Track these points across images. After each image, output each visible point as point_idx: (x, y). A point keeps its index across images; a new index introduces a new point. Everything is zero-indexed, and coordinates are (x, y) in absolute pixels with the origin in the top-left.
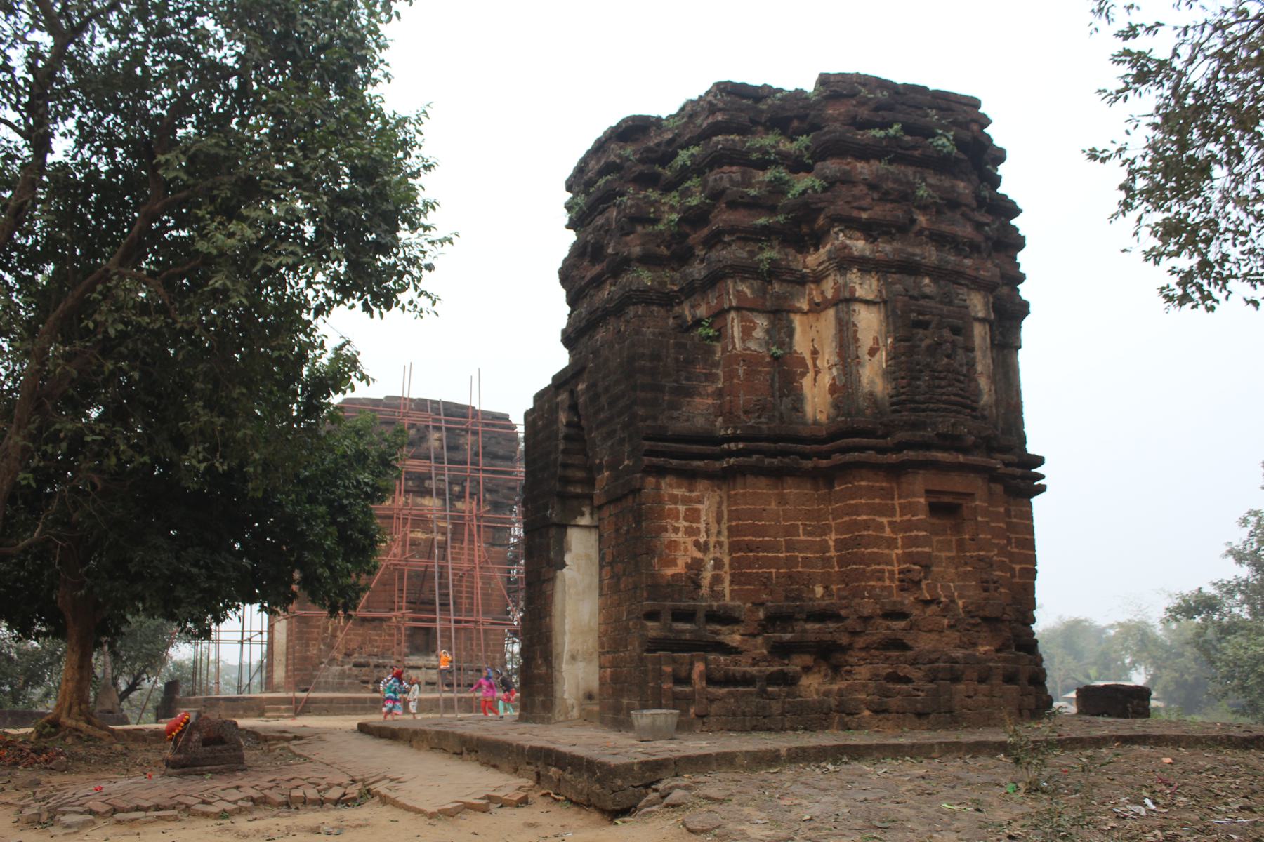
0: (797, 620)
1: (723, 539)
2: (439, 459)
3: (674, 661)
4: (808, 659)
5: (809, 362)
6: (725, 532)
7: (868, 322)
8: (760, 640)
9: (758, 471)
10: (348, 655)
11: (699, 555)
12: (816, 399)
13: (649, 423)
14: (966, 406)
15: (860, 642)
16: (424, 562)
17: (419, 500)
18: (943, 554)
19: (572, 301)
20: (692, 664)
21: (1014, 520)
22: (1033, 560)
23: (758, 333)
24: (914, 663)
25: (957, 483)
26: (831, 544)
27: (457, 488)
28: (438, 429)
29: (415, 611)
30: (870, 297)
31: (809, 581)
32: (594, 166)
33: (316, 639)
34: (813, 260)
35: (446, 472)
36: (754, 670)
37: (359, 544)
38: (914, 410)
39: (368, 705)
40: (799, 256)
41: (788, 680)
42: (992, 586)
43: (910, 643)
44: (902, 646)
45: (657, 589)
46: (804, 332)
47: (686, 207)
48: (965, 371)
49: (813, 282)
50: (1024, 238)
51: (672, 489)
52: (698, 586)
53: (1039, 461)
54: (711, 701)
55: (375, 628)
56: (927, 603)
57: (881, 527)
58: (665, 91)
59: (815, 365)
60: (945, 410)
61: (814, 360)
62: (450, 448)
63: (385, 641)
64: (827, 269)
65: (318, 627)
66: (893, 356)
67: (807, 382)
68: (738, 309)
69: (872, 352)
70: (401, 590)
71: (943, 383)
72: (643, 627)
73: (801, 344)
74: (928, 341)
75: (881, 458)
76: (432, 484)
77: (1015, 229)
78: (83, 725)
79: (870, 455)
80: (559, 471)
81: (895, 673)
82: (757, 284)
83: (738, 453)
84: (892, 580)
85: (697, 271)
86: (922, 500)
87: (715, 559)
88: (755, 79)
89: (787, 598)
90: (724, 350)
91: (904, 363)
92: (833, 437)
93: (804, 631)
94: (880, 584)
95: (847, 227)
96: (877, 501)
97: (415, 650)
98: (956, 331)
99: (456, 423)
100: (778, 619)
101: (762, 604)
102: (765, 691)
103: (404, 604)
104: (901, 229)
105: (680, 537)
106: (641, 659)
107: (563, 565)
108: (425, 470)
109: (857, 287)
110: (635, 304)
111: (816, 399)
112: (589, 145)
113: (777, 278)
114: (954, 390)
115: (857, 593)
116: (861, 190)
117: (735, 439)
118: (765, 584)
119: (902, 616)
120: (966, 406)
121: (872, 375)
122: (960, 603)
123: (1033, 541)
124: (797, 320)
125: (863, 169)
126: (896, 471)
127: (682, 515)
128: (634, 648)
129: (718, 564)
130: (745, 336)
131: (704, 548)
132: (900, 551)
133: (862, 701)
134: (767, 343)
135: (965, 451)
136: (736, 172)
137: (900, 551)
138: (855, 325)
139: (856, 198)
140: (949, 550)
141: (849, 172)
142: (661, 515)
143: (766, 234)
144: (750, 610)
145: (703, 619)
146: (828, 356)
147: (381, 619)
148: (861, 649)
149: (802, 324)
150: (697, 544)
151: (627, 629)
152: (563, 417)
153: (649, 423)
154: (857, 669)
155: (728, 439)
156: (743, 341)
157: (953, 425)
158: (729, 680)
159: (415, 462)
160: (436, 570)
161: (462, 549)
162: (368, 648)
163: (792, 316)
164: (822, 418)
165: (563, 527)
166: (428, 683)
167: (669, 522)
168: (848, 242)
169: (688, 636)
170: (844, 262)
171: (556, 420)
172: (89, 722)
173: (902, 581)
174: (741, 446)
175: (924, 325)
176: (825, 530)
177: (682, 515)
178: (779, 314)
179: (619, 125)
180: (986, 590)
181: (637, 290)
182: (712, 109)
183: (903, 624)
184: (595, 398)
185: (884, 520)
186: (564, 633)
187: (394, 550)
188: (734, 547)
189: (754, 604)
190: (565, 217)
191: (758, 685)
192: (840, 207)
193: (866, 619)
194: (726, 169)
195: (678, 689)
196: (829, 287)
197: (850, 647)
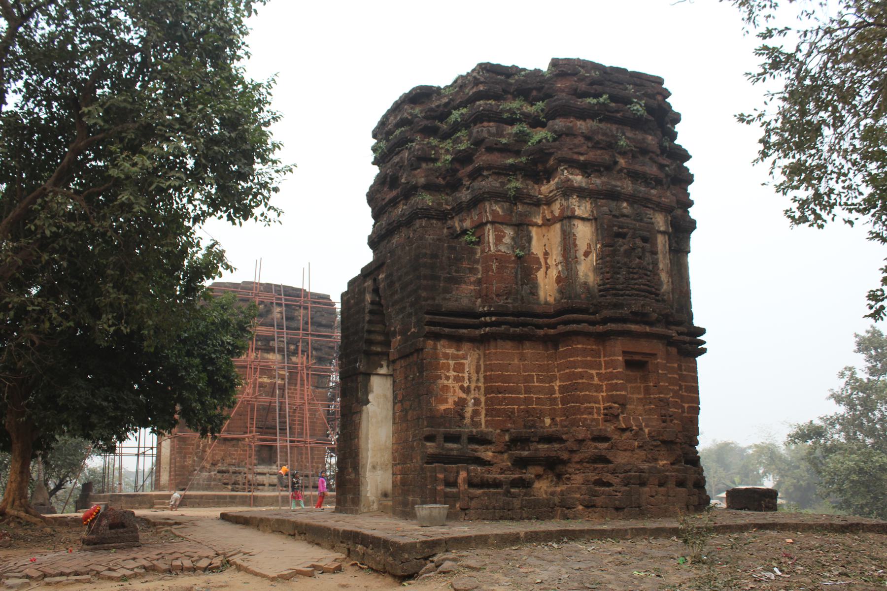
0: (532, 442)
2: (280, 326)
3: (445, 470)
4: (539, 470)
5: (542, 261)
6: (482, 380)
7: (584, 233)
8: (506, 456)
11: (464, 396)
12: (547, 286)
13: (429, 302)
14: (651, 293)
15: (576, 457)
16: (268, 399)
17: (266, 355)
19: (376, 216)
20: (458, 473)
23: (507, 240)
24: (614, 472)
25: (644, 346)
26: (557, 388)
27: (292, 347)
28: (280, 305)
30: (585, 215)
31: (541, 414)
32: (392, 120)
33: (191, 453)
34: (546, 189)
36: (502, 477)
39: (228, 500)
40: (536, 186)
41: (526, 484)
43: (611, 459)
44: (605, 460)
45: (434, 419)
46: (539, 240)
49: (545, 204)
51: (445, 349)
53: (702, 331)
54: (472, 499)
55: (233, 446)
56: (623, 430)
57: (591, 377)
59: (546, 263)
61: (546, 259)
65: (193, 445)
66: (600, 257)
67: (540, 274)
69: (586, 254)
70: (252, 419)
71: (636, 276)
72: (424, 446)
73: (537, 248)
74: (626, 247)
75: (591, 329)
76: (275, 344)
77: (687, 169)
79: (584, 327)
80: (366, 336)
82: (506, 205)
83: (491, 324)
84: (599, 414)
85: (464, 195)
86: (620, 358)
87: (475, 399)
88: (506, 61)
89: (525, 426)
90: (483, 251)
91: (608, 263)
92: (559, 313)
93: (537, 450)
94: (590, 417)
95: (569, 166)
96: (589, 358)
97: (262, 461)
98: (645, 240)
99: (292, 301)
100: (518, 441)
101: (507, 431)
102: (509, 492)
103: (254, 429)
104: (609, 168)
105: (450, 383)
106: (422, 469)
107: (368, 402)
108: (270, 334)
109: (576, 208)
110: (420, 218)
111: (547, 286)
112: (389, 105)
115: (574, 423)
116: (580, 140)
117: (489, 314)
119: (606, 439)
120: (651, 293)
121: (586, 270)
122: (646, 430)
123: (697, 387)
124: (534, 231)
125: (582, 126)
126: (603, 338)
127: (452, 367)
129: (477, 402)
130: (498, 242)
131: (467, 391)
132: (604, 394)
133: (577, 499)
135: (651, 324)
136: (492, 126)
137: (604, 394)
138: (574, 235)
139: (576, 146)
141: (572, 127)
143: (513, 170)
144: (499, 434)
145: (466, 441)
146: (556, 256)
147: (238, 440)
148: (577, 463)
149: (537, 234)
150: (462, 388)
151: (412, 448)
154: (574, 476)
155: (485, 314)
156: (496, 245)
157: (643, 306)
159: (263, 328)
161: (296, 390)
163: (530, 228)
164: (551, 300)
165: (368, 375)
166: (270, 485)
168: (570, 177)
169: (455, 453)
170: (568, 190)
171: (363, 300)
173: (606, 415)
174: (494, 319)
175: (623, 236)
176: (552, 379)
177: (452, 367)
178: (522, 227)
179: (411, 92)
180: (664, 422)
181: (422, 209)
182: (476, 82)
183: (606, 445)
184: (391, 284)
185: (594, 372)
186: (368, 450)
188: (488, 390)
189: (502, 430)
191: (504, 487)
192: (565, 152)
193: (581, 442)
194: (485, 124)
195: (448, 490)
196: (556, 208)
197: (569, 461)
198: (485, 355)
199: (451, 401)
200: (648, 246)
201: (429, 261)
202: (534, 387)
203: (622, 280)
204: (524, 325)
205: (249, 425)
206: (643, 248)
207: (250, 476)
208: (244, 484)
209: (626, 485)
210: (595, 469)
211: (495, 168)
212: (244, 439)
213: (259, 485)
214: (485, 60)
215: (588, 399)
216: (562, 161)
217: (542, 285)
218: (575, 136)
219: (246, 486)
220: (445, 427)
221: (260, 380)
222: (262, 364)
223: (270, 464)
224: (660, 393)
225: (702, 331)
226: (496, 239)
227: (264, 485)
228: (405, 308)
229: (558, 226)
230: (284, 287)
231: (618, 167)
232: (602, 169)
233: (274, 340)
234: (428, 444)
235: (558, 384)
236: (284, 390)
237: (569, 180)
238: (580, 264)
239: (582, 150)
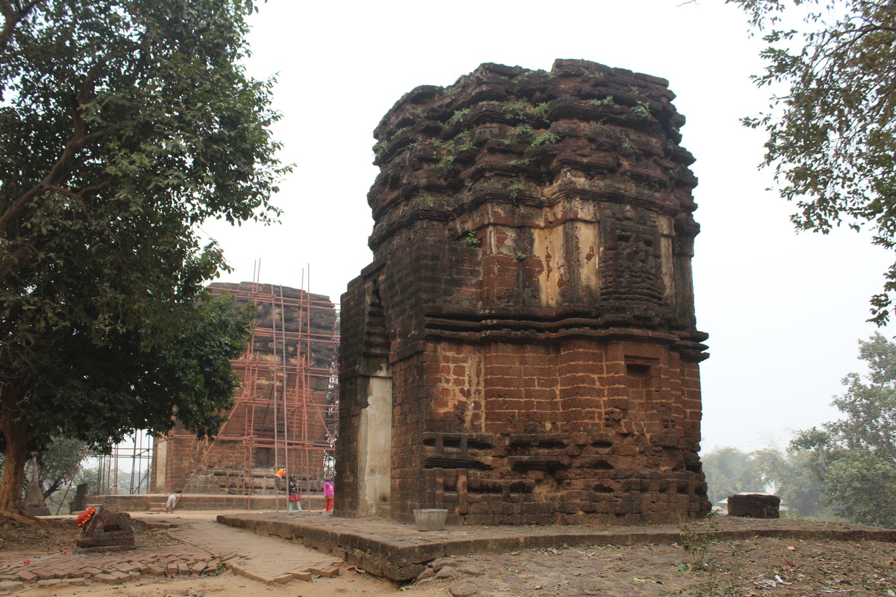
2: (279, 328)
3: (445, 474)
4: (540, 474)
5: (544, 264)
6: (482, 383)
7: (587, 236)
8: (506, 460)
10: (210, 467)
11: (464, 399)
12: (549, 289)
13: (430, 304)
14: (654, 297)
15: (577, 463)
16: (266, 401)
17: (265, 357)
19: (377, 216)
20: (457, 477)
22: (699, 406)
23: (509, 242)
24: (615, 478)
25: (647, 351)
26: (558, 392)
27: (291, 349)
28: (279, 306)
30: (588, 218)
31: (542, 419)
32: (394, 121)
34: (548, 191)
36: (501, 482)
37: (220, 388)
38: (618, 299)
39: (225, 503)
40: (539, 188)
41: (525, 489)
43: (612, 464)
45: (433, 423)
46: (541, 242)
49: (548, 207)
51: (445, 352)
53: (705, 336)
54: (471, 503)
55: (230, 448)
56: (625, 435)
57: (593, 381)
59: (548, 266)
60: (640, 299)
61: (548, 262)
62: (287, 320)
63: (237, 457)
65: (190, 447)
66: (603, 261)
67: (542, 277)
68: (494, 225)
69: (589, 257)
71: (639, 280)
72: (423, 450)
73: (539, 251)
74: (628, 250)
75: (593, 332)
76: (274, 346)
77: (691, 173)
80: (365, 338)
82: (508, 207)
83: (492, 327)
84: (600, 419)
85: (466, 197)
86: (622, 363)
87: (475, 402)
88: (510, 62)
89: (525, 431)
90: (484, 253)
91: (611, 266)
92: (560, 317)
93: (537, 454)
94: (592, 421)
95: (572, 168)
96: (590, 363)
98: (648, 243)
99: (291, 302)
101: (508, 435)
102: (509, 497)
103: (252, 431)
104: (612, 170)
105: (450, 386)
106: (421, 473)
107: (367, 405)
109: (579, 211)
110: (421, 219)
111: (549, 289)
115: (575, 428)
119: (607, 444)
120: (654, 297)
121: (589, 273)
122: (648, 436)
124: (536, 233)
125: (585, 127)
126: (604, 342)
127: (452, 371)
128: (417, 465)
129: (477, 406)
130: (500, 244)
131: (467, 394)
132: (606, 399)
133: (578, 505)
134: (515, 249)
136: (495, 127)
137: (606, 399)
138: (577, 238)
139: (580, 148)
143: (516, 172)
144: (499, 439)
145: (465, 445)
146: (558, 259)
147: (235, 442)
148: (577, 467)
149: (539, 236)
150: (462, 391)
151: (412, 452)
153: (430, 304)
154: (574, 482)
155: (486, 317)
156: (498, 247)
157: (645, 310)
159: (262, 329)
161: (294, 392)
163: (533, 230)
164: (552, 303)
165: (367, 378)
166: (268, 488)
167: (443, 376)
168: (573, 179)
169: (455, 457)
170: (571, 193)
171: (364, 302)
173: (607, 419)
174: (495, 322)
175: (626, 239)
176: (553, 383)
177: (452, 371)
178: (524, 229)
179: (413, 92)
180: (666, 427)
183: (607, 450)
184: (391, 286)
185: (595, 376)
188: (488, 394)
189: (502, 434)
190: (372, 157)
192: (568, 154)
194: (488, 125)
195: (447, 494)
196: (559, 211)
197: (569, 466)
198: (486, 358)
199: (450, 404)
200: (651, 249)
201: (430, 263)
204: (525, 328)
205: (246, 428)
207: (247, 479)
209: (627, 491)
210: (596, 474)
212: (241, 441)
213: (256, 488)
216: (565, 163)
218: (578, 138)
219: (244, 489)
221: (258, 382)
223: (268, 467)
227: (261, 488)
230: (283, 287)
234: (428, 448)
236: (282, 392)
239: (585, 152)
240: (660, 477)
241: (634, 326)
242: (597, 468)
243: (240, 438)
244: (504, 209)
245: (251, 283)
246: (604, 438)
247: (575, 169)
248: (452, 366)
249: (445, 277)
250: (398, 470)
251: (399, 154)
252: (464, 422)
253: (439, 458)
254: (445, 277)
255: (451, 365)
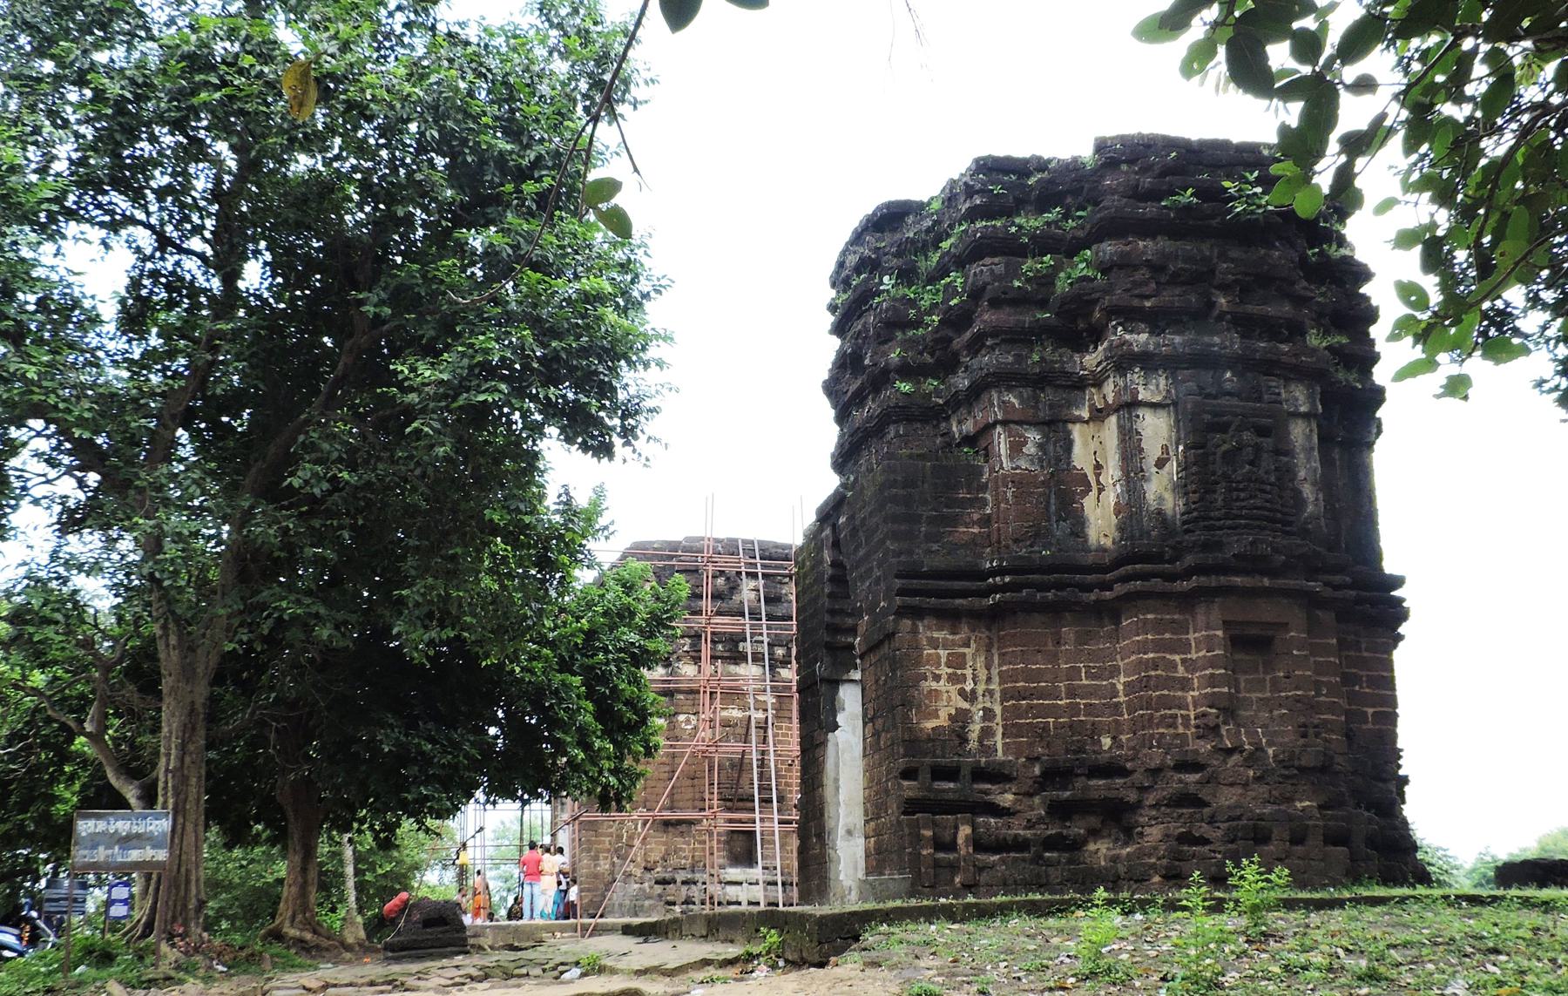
0: (1078, 775)
1: (994, 686)
2: (755, 615)
3: (935, 824)
4: (1094, 821)
5: (1092, 478)
6: (996, 679)
7: (1155, 429)
8: (1037, 800)
9: (1030, 608)
11: (966, 705)
12: (1100, 519)
13: (903, 558)
14: (1273, 521)
15: (1151, 799)
16: (738, 747)
17: (732, 668)
18: (1254, 696)
19: (841, 418)
20: (957, 828)
21: (1366, 654)
22: (1392, 702)
23: (1030, 449)
24: (1212, 821)
25: (1266, 612)
26: (1120, 687)
27: (780, 652)
28: (754, 576)
29: (729, 810)
30: (1157, 399)
31: (1095, 731)
32: (852, 260)
34: (1092, 360)
35: (765, 631)
36: (1028, 833)
37: (624, 722)
38: (1206, 528)
40: (1077, 358)
41: (1076, 845)
42: (1311, 731)
43: (1207, 799)
44: (1196, 802)
45: (914, 743)
46: (1085, 444)
47: (969, 303)
48: (1273, 479)
49: (1093, 385)
50: (1377, 308)
51: (929, 631)
52: (964, 740)
53: (1398, 582)
54: (981, 870)
56: (1230, 752)
57: (1173, 666)
58: (925, 175)
59: (1098, 482)
60: (1246, 526)
61: (1098, 475)
62: (769, 601)
64: (1105, 370)
65: (611, 835)
66: (1184, 467)
67: (1089, 502)
68: (1004, 423)
69: (1160, 463)
71: (1242, 495)
72: (900, 787)
73: (1081, 458)
74: (1226, 447)
75: (1168, 586)
76: (747, 647)
77: (1366, 299)
78: (308, 936)
79: (1156, 584)
80: (827, 618)
81: (1189, 833)
82: (1027, 392)
83: (1003, 588)
84: (1186, 725)
85: (962, 382)
86: (1220, 633)
87: (984, 709)
88: (1020, 150)
89: (1067, 751)
90: (992, 470)
91: (1200, 473)
92: (1118, 563)
93: (1086, 788)
94: (1172, 731)
95: (1127, 320)
96: (1167, 636)
98: (1263, 432)
99: (776, 567)
100: (1054, 775)
101: (1037, 759)
102: (1041, 857)
103: (715, 802)
104: (1200, 316)
105: (942, 685)
106: (899, 822)
107: (836, 727)
108: (737, 629)
109: (1141, 389)
110: (895, 422)
111: (1100, 519)
112: (847, 235)
113: (1050, 383)
114: (1258, 502)
115: (1146, 742)
116: (1142, 274)
117: (1000, 571)
118: (1041, 736)
119: (1196, 767)
120: (1273, 521)
121: (1161, 489)
122: (1270, 751)
123: (1392, 679)
124: (1077, 431)
125: (1146, 247)
126: (1188, 601)
127: (943, 660)
128: (893, 808)
129: (988, 714)
130: (1011, 455)
131: (971, 697)
132: (1196, 693)
133: (1153, 866)
134: (1041, 460)
135: (1272, 574)
136: (996, 264)
137: (1196, 693)
138: (1139, 433)
139: (1136, 284)
140: (1262, 690)
141: (1128, 253)
142: (918, 662)
143: (1041, 332)
144: (1024, 766)
145: (968, 777)
146: (1112, 472)
147: (690, 823)
148: (1152, 807)
149: (1082, 435)
150: (962, 693)
151: (887, 791)
152: (827, 556)
153: (903, 558)
154: (1147, 830)
155: (993, 573)
156: (1011, 458)
157: (1252, 543)
158: (1000, 846)
159: (726, 620)
160: (754, 757)
161: (790, 729)
162: (674, 861)
163: (1070, 426)
164: (1108, 543)
165: (835, 684)
167: (926, 669)
168: (1127, 337)
169: (951, 796)
170: (1123, 361)
171: (821, 561)
172: (315, 932)
173: (1197, 727)
174: (1007, 579)
175: (1223, 428)
176: (1115, 672)
177: (943, 660)
178: (1056, 427)
179: (874, 214)
180: (1304, 736)
181: (897, 406)
182: (970, 191)
183: (1195, 777)
184: (854, 532)
185: (1177, 658)
186: (839, 804)
187: (701, 734)
188: (1006, 696)
189: (1028, 759)
190: (829, 319)
191: (1033, 849)
192: (1118, 296)
193: (1155, 772)
194: (988, 260)
195: (941, 855)
196: (1109, 389)
197: (1138, 805)
198: (1000, 639)
199: (943, 714)
200: (1267, 443)
201: (901, 492)
202: (1080, 686)
203: (1220, 503)
204: (1060, 586)
205: (707, 796)
206: (1258, 449)
208: (703, 903)
209: (1232, 842)
210: (1180, 816)
211: (1005, 332)
212: (700, 821)
214: (984, 152)
215: (1165, 703)
216: (1112, 312)
217: (1092, 519)
218: (1136, 268)
220: (935, 756)
221: (724, 713)
222: (723, 684)
224: (1297, 688)
225: (1398, 582)
226: (1011, 448)
228: (871, 569)
229: (1113, 419)
231: (1216, 313)
232: (1185, 319)
233: (744, 640)
234: (906, 783)
235: (1122, 680)
236: (765, 729)
237: (1126, 342)
238: (1147, 480)
239: (1146, 290)
240: (1291, 818)
241: (1237, 573)
242: (1182, 806)
243: (694, 815)
244: (1020, 397)
245: (703, 539)
246: (1189, 758)
247: (1132, 320)
248: (943, 653)
249: (926, 512)
250: (872, 824)
251: (859, 317)
252: (967, 741)
253: (924, 798)
254: (926, 512)
255: (941, 652)
